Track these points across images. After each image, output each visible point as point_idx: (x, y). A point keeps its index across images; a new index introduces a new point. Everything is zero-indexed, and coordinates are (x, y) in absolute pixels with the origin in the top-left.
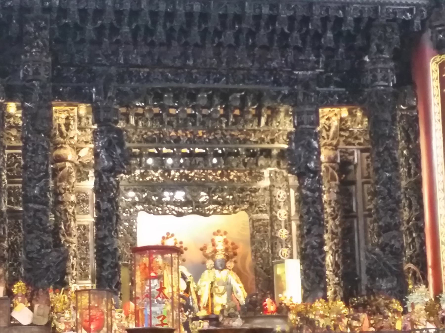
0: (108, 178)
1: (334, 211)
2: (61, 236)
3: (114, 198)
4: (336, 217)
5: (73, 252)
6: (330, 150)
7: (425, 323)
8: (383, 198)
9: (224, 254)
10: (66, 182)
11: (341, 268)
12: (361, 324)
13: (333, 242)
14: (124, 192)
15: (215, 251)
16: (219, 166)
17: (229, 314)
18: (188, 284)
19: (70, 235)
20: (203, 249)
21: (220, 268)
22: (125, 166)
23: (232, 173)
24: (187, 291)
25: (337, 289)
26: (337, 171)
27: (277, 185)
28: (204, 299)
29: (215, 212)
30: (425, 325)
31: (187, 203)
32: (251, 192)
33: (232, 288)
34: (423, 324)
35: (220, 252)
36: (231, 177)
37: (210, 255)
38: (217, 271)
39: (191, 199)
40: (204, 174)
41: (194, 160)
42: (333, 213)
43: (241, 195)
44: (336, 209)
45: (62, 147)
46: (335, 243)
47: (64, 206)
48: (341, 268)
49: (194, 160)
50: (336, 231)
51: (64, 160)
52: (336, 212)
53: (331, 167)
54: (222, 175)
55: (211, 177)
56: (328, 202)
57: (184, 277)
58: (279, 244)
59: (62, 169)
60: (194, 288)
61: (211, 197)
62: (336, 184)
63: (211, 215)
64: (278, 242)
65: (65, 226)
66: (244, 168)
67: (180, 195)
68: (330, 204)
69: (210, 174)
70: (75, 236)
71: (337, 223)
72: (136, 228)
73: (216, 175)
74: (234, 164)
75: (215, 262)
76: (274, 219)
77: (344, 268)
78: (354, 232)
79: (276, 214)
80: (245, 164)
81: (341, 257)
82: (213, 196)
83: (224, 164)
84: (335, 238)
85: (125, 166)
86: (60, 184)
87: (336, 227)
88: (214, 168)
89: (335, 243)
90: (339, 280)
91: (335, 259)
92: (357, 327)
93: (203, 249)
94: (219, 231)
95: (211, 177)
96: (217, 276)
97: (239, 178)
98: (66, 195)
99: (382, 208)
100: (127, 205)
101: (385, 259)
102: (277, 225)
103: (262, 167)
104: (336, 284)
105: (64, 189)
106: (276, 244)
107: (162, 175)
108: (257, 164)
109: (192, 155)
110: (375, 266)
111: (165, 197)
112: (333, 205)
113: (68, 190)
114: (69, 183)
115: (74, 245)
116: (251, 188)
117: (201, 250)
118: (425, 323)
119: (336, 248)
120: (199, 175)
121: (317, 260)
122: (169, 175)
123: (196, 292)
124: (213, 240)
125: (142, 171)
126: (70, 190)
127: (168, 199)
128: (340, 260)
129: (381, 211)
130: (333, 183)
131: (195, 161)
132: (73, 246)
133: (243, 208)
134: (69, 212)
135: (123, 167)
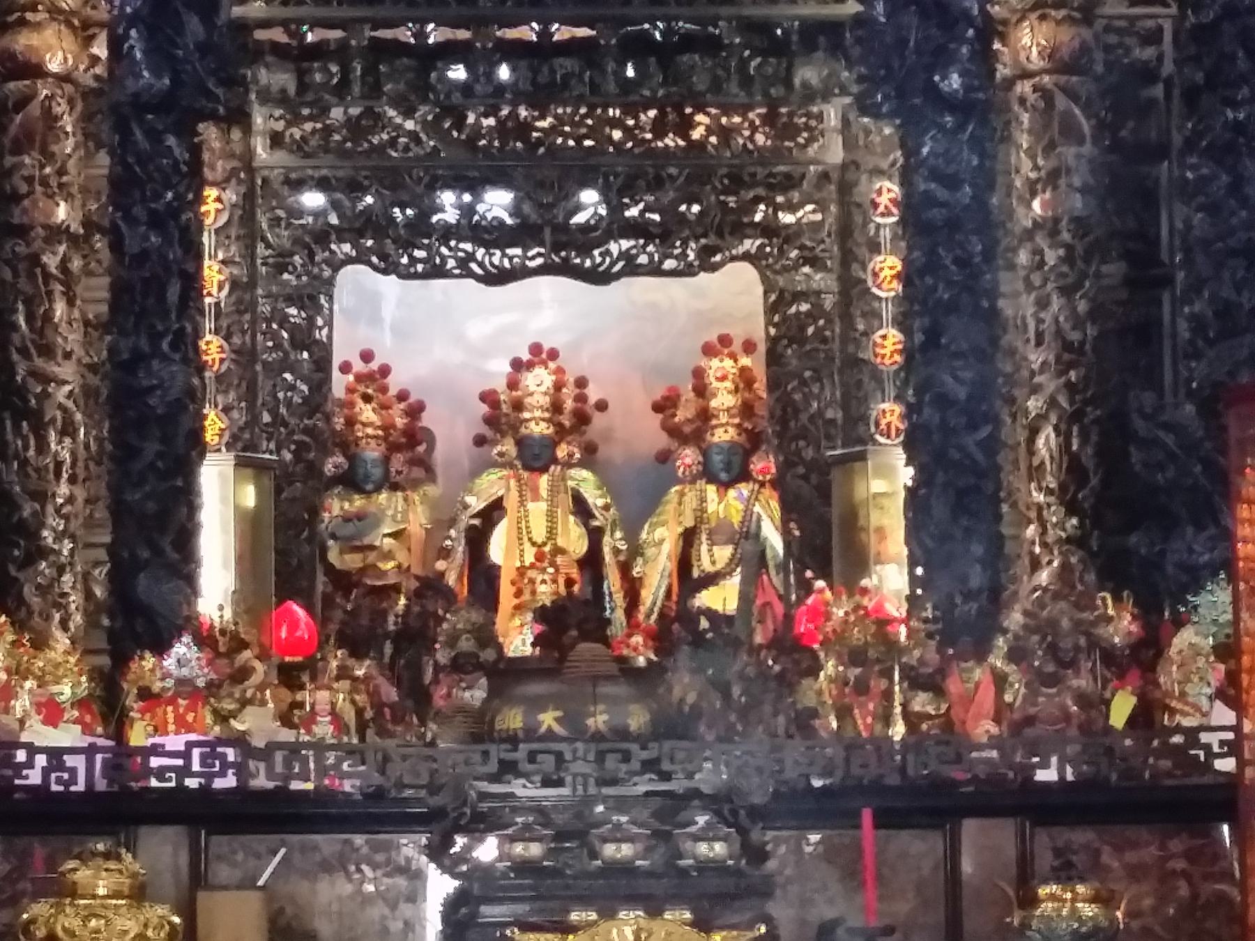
0: (155, 137)
1: (1069, 259)
2: (15, 357)
3: (174, 212)
4: (1078, 286)
5: (59, 414)
6: (1058, 23)
7: (1205, 703)
8: (1212, 209)
9: (738, 426)
10: (35, 154)
11: (1094, 481)
12: (944, 707)
13: (1063, 380)
14: (285, 191)
15: (705, 416)
16: (647, 93)
17: (454, 660)
18: (595, 536)
19: (47, 351)
20: (665, 405)
21: (723, 476)
22: (219, 91)
23: (700, 118)
24: (591, 562)
25: (1073, 560)
26: (1086, 108)
27: (869, 162)
28: (654, 589)
29: (632, 269)
30: (1205, 715)
31: (522, 233)
32: (771, 187)
33: (763, 553)
34: (1198, 708)
35: (724, 418)
36: (696, 134)
37: (687, 429)
38: (711, 490)
39: (534, 217)
40: (590, 122)
41: (545, 70)
42: (1065, 269)
43: (732, 201)
44: (1079, 249)
45: (23, 23)
46: (1069, 386)
47: (28, 245)
48: (1094, 481)
49: (545, 70)
50: (1075, 336)
51: (36, 71)
52: (1080, 263)
53: (1065, 90)
54: (659, 129)
55: (617, 135)
56: (1049, 225)
57: (581, 508)
58: (869, 385)
59: (24, 101)
60: (616, 551)
61: (616, 209)
62: (1078, 156)
63: (618, 276)
64: (866, 380)
65: (30, 318)
66: (742, 97)
67: (497, 203)
68: (1054, 233)
69: (616, 123)
70: (68, 355)
71: (1082, 306)
72: (329, 323)
73: (637, 126)
74: (700, 82)
75: (705, 453)
76: (855, 292)
77: (1106, 483)
78: (1161, 343)
79: (861, 275)
80: (746, 82)
81: (1094, 438)
82: (628, 207)
83: (665, 83)
84: (1071, 365)
85: (219, 91)
86: (15, 159)
87: (1078, 323)
88: (631, 100)
89: (1069, 386)
90: (1081, 525)
91: (1068, 444)
92: (929, 717)
93: (665, 405)
94: (725, 340)
95: (617, 135)
96: (712, 507)
97: (726, 134)
98: (35, 203)
99: (1206, 243)
100: (296, 241)
101: (1208, 445)
102: (864, 315)
103: (810, 95)
104: (1069, 540)
105: (29, 180)
106: (859, 384)
107: (432, 127)
108: (788, 83)
109: (543, 50)
110: (1171, 473)
111: (442, 210)
112: (1066, 236)
113: (44, 182)
114: (49, 157)
115: (67, 388)
116: (771, 175)
117: (657, 408)
118: (1205, 703)
119: (1071, 403)
120: (573, 124)
121: (961, 449)
122: (460, 123)
123: (625, 569)
124: (699, 374)
125: (355, 111)
126: (54, 182)
127: (450, 215)
128: (1090, 450)
129: (1200, 258)
130: (1069, 152)
131: (553, 72)
132: (61, 395)
133: (741, 250)
134: (44, 267)
135: (209, 95)
